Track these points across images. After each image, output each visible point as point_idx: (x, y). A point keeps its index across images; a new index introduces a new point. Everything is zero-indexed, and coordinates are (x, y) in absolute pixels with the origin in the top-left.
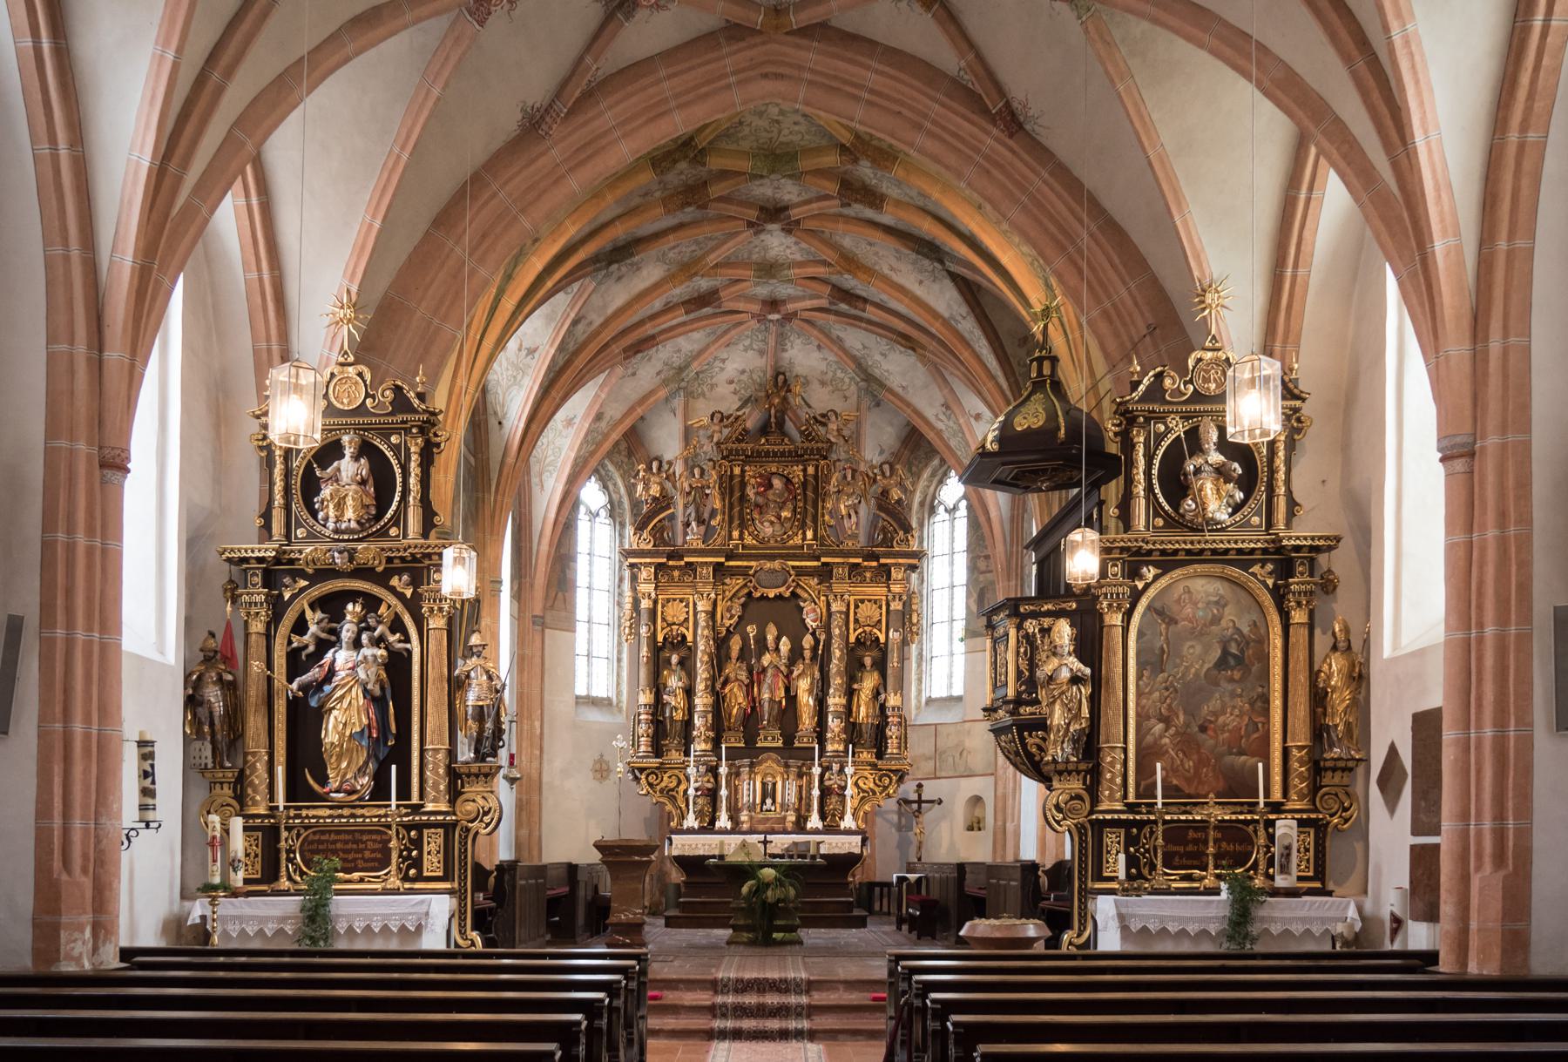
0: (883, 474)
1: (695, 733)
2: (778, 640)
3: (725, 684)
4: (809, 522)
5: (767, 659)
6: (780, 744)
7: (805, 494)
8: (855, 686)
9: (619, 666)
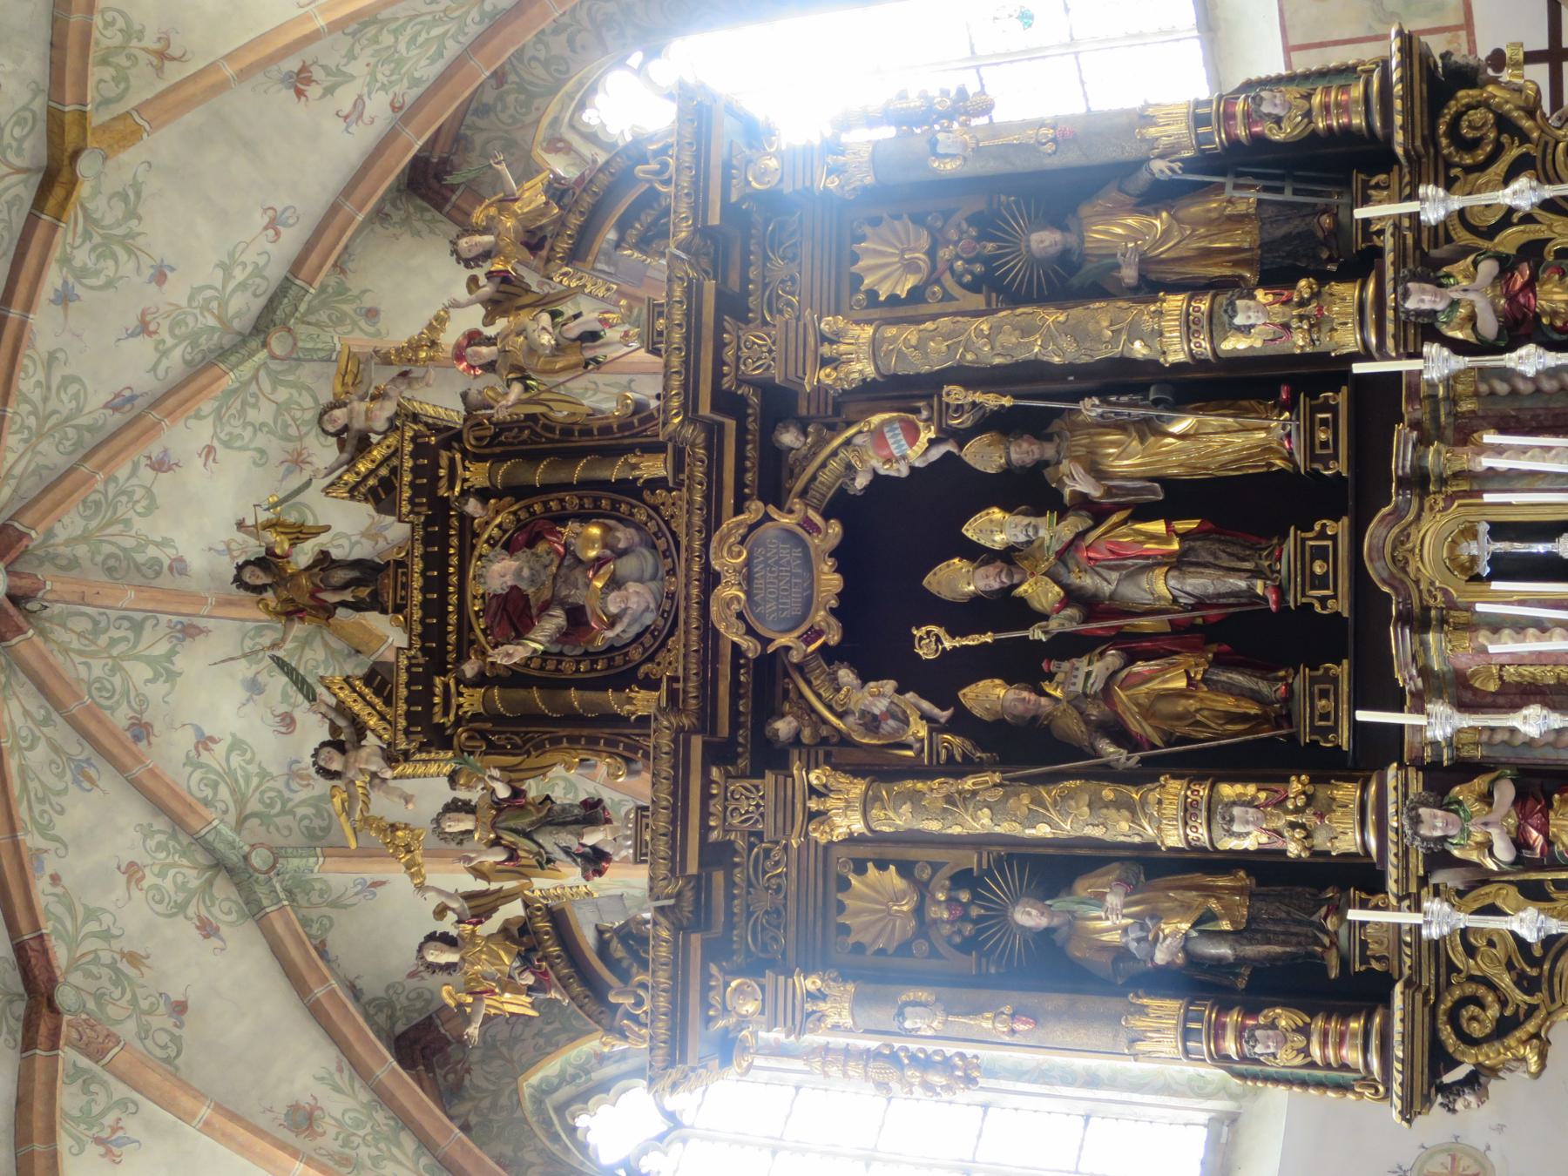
0: (487, 255)
1: (1293, 850)
2: (976, 554)
3: (1120, 734)
4: (615, 473)
5: (1040, 592)
6: (1340, 528)
7: (547, 488)
8: (1129, 274)
9: (1113, 1083)
